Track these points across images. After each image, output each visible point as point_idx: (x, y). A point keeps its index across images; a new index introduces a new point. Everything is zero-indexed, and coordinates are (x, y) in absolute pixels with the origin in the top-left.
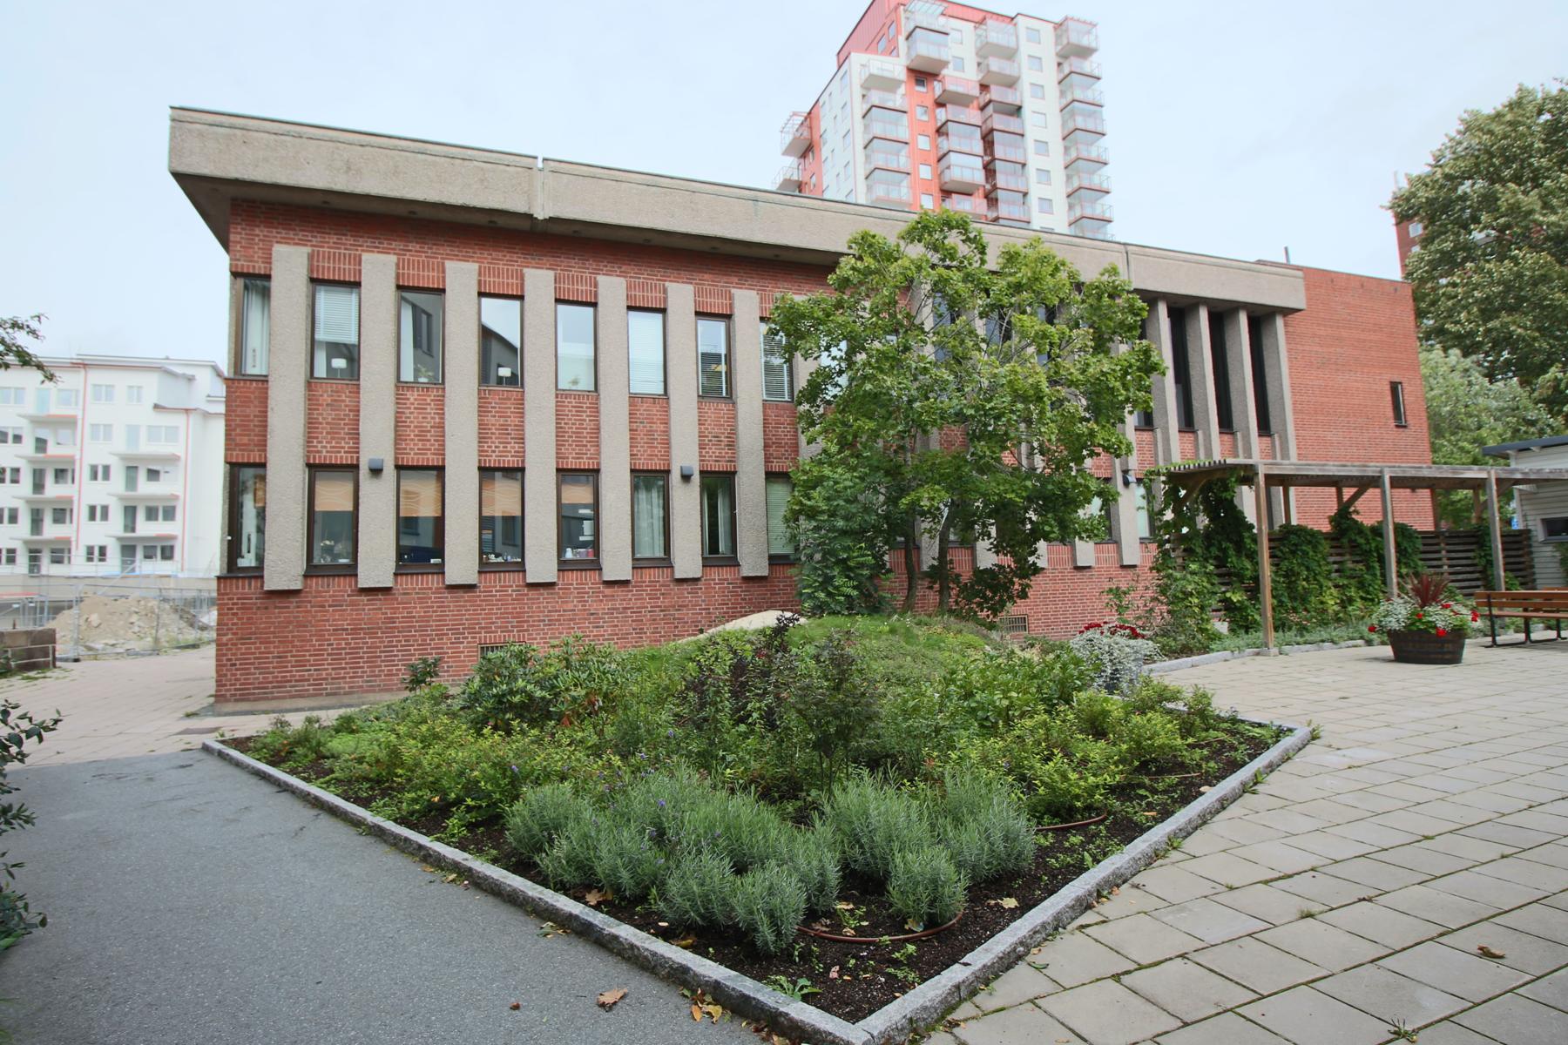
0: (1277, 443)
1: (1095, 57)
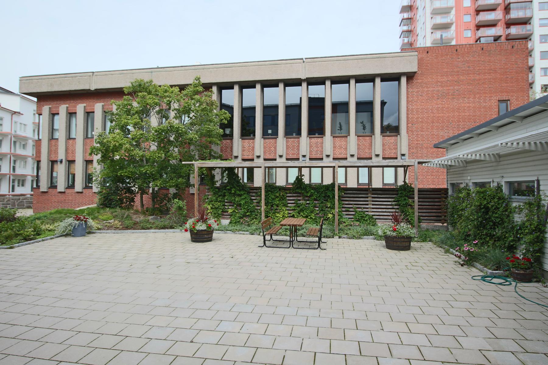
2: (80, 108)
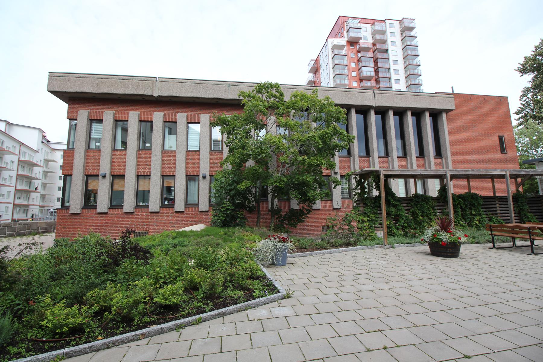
0: (444, 161)
1: (415, 30)
2: (133, 116)
